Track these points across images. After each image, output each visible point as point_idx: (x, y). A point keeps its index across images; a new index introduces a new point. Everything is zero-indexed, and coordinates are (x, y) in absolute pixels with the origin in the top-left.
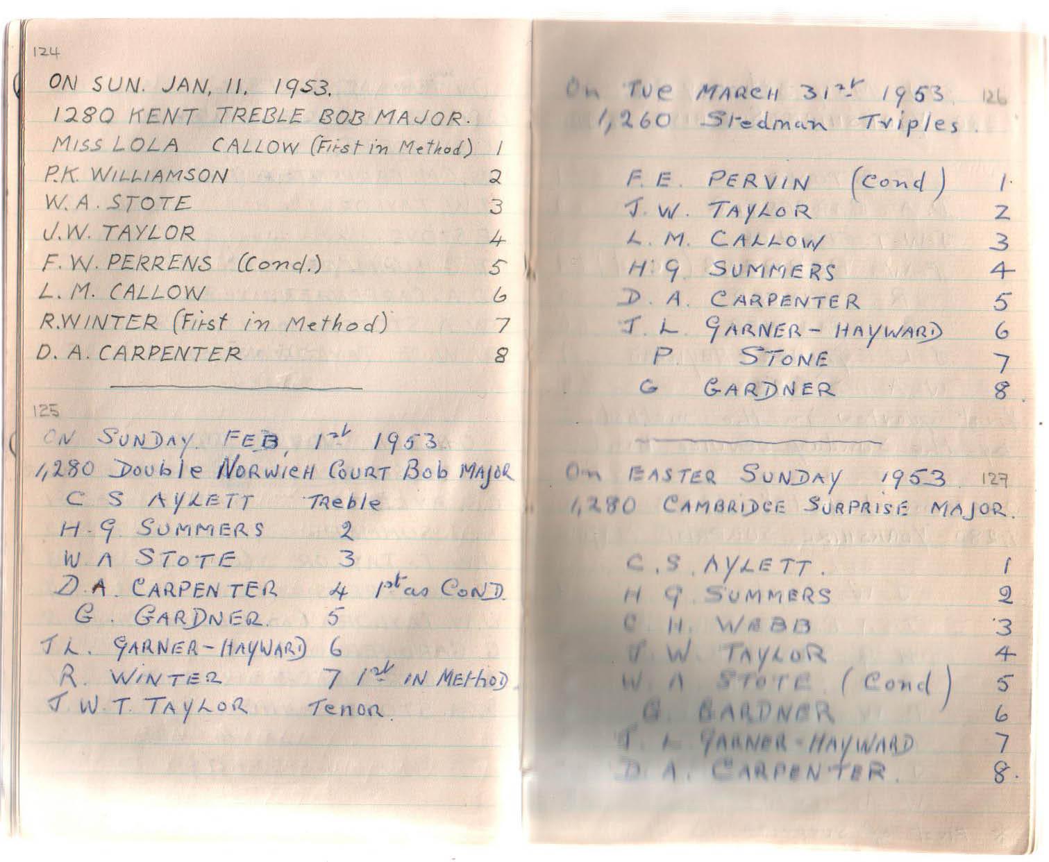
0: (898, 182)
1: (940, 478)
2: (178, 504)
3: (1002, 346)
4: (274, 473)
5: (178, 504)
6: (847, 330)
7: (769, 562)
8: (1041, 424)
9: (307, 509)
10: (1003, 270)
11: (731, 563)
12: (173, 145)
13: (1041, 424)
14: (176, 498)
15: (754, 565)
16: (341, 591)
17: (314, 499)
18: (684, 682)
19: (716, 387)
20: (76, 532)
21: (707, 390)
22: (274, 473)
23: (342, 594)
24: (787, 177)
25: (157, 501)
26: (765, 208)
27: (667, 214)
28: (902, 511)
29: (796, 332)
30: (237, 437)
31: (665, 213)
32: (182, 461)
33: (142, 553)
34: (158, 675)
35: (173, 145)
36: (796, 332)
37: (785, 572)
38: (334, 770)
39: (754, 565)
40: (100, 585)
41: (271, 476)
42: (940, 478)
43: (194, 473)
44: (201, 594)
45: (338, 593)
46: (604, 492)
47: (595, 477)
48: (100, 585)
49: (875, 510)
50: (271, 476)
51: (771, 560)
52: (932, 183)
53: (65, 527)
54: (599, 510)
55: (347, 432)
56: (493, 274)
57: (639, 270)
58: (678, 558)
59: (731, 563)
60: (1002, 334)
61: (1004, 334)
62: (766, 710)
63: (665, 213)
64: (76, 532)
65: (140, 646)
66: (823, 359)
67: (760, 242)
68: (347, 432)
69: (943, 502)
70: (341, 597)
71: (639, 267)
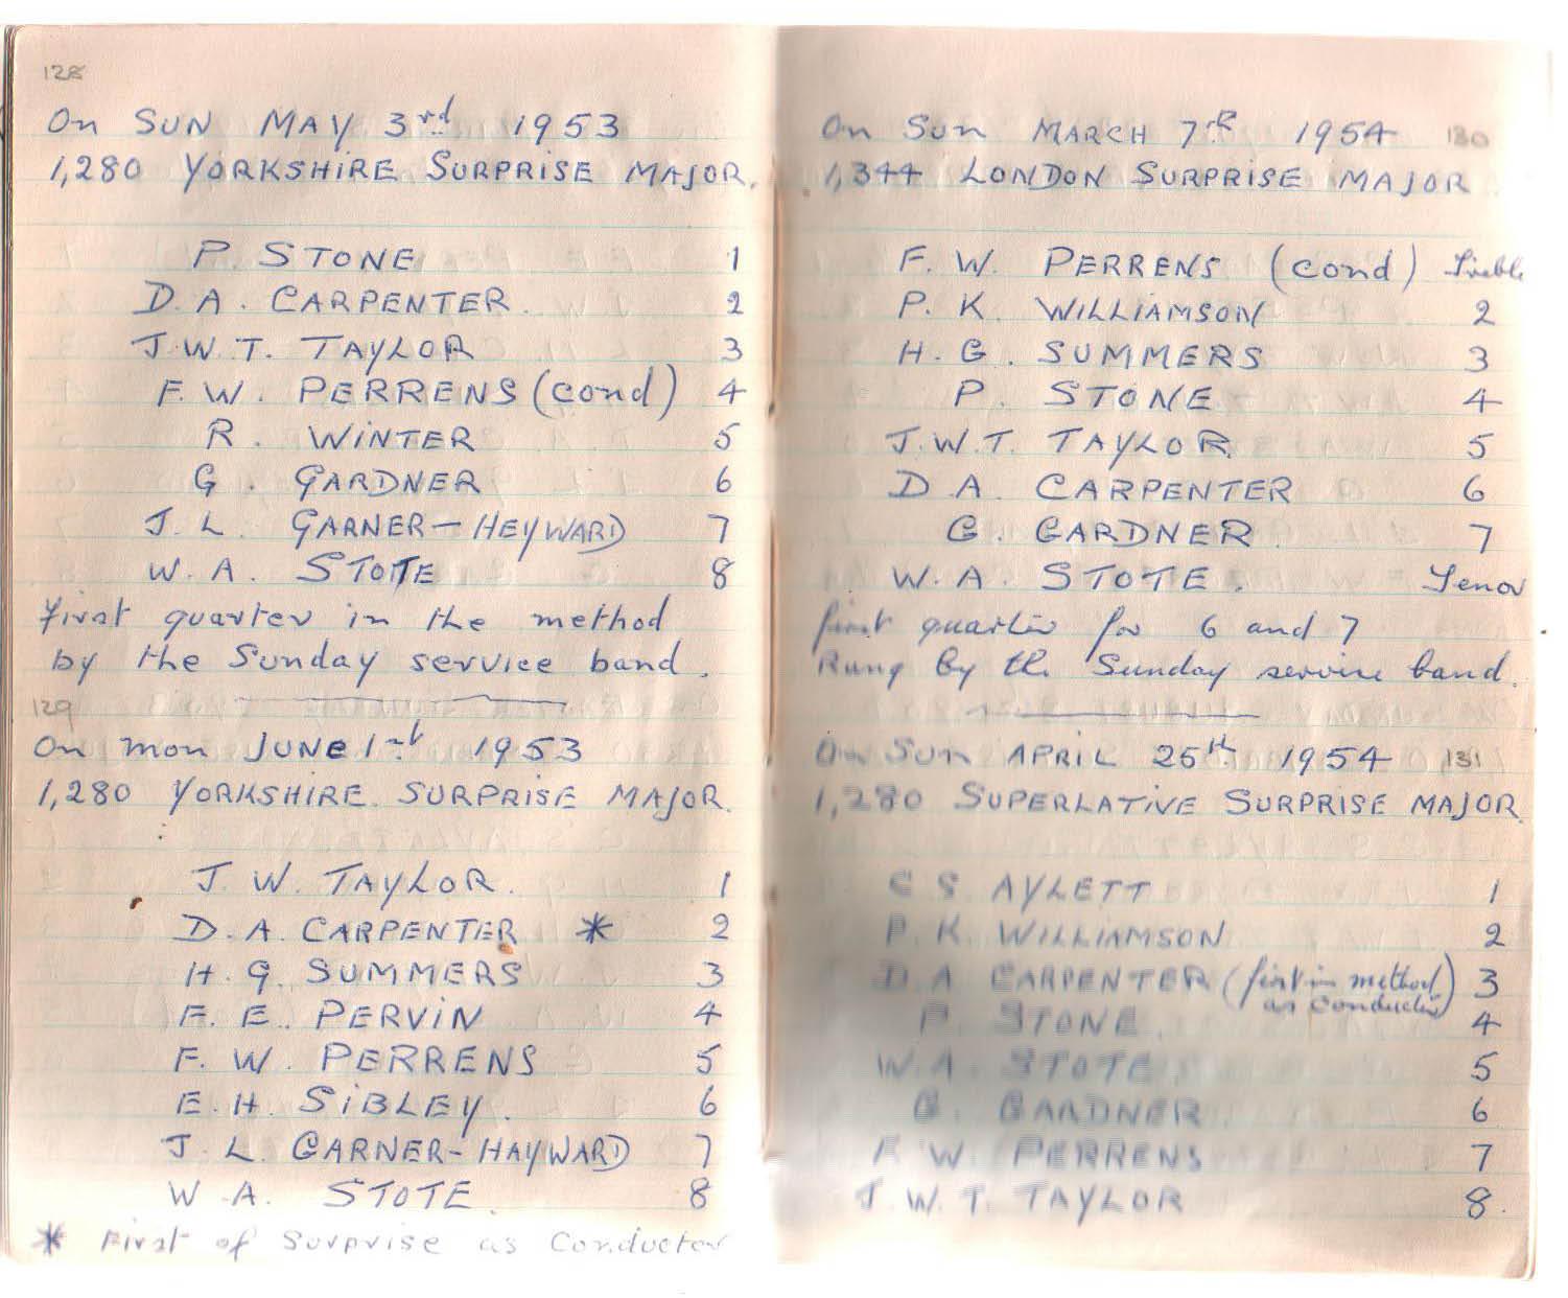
0: (638, 662)
3: (1478, 513)
8: (1544, 632)
10: (1481, 401)
11: (1033, 885)
13: (1544, 632)
15: (1068, 887)
18: (877, 1063)
27: (1058, 314)
28: (565, 801)
31: (1055, 313)
32: (167, 646)
33: (1056, 389)
38: (355, 548)
39: (1068, 887)
43: (189, 666)
44: (255, 1016)
46: (868, 780)
51: (1091, 880)
52: (1398, 270)
54: (867, 807)
55: (1178, 271)
58: (954, 878)
59: (1033, 885)
60: (1472, 495)
61: (1478, 496)
63: (1055, 313)
68: (1178, 271)
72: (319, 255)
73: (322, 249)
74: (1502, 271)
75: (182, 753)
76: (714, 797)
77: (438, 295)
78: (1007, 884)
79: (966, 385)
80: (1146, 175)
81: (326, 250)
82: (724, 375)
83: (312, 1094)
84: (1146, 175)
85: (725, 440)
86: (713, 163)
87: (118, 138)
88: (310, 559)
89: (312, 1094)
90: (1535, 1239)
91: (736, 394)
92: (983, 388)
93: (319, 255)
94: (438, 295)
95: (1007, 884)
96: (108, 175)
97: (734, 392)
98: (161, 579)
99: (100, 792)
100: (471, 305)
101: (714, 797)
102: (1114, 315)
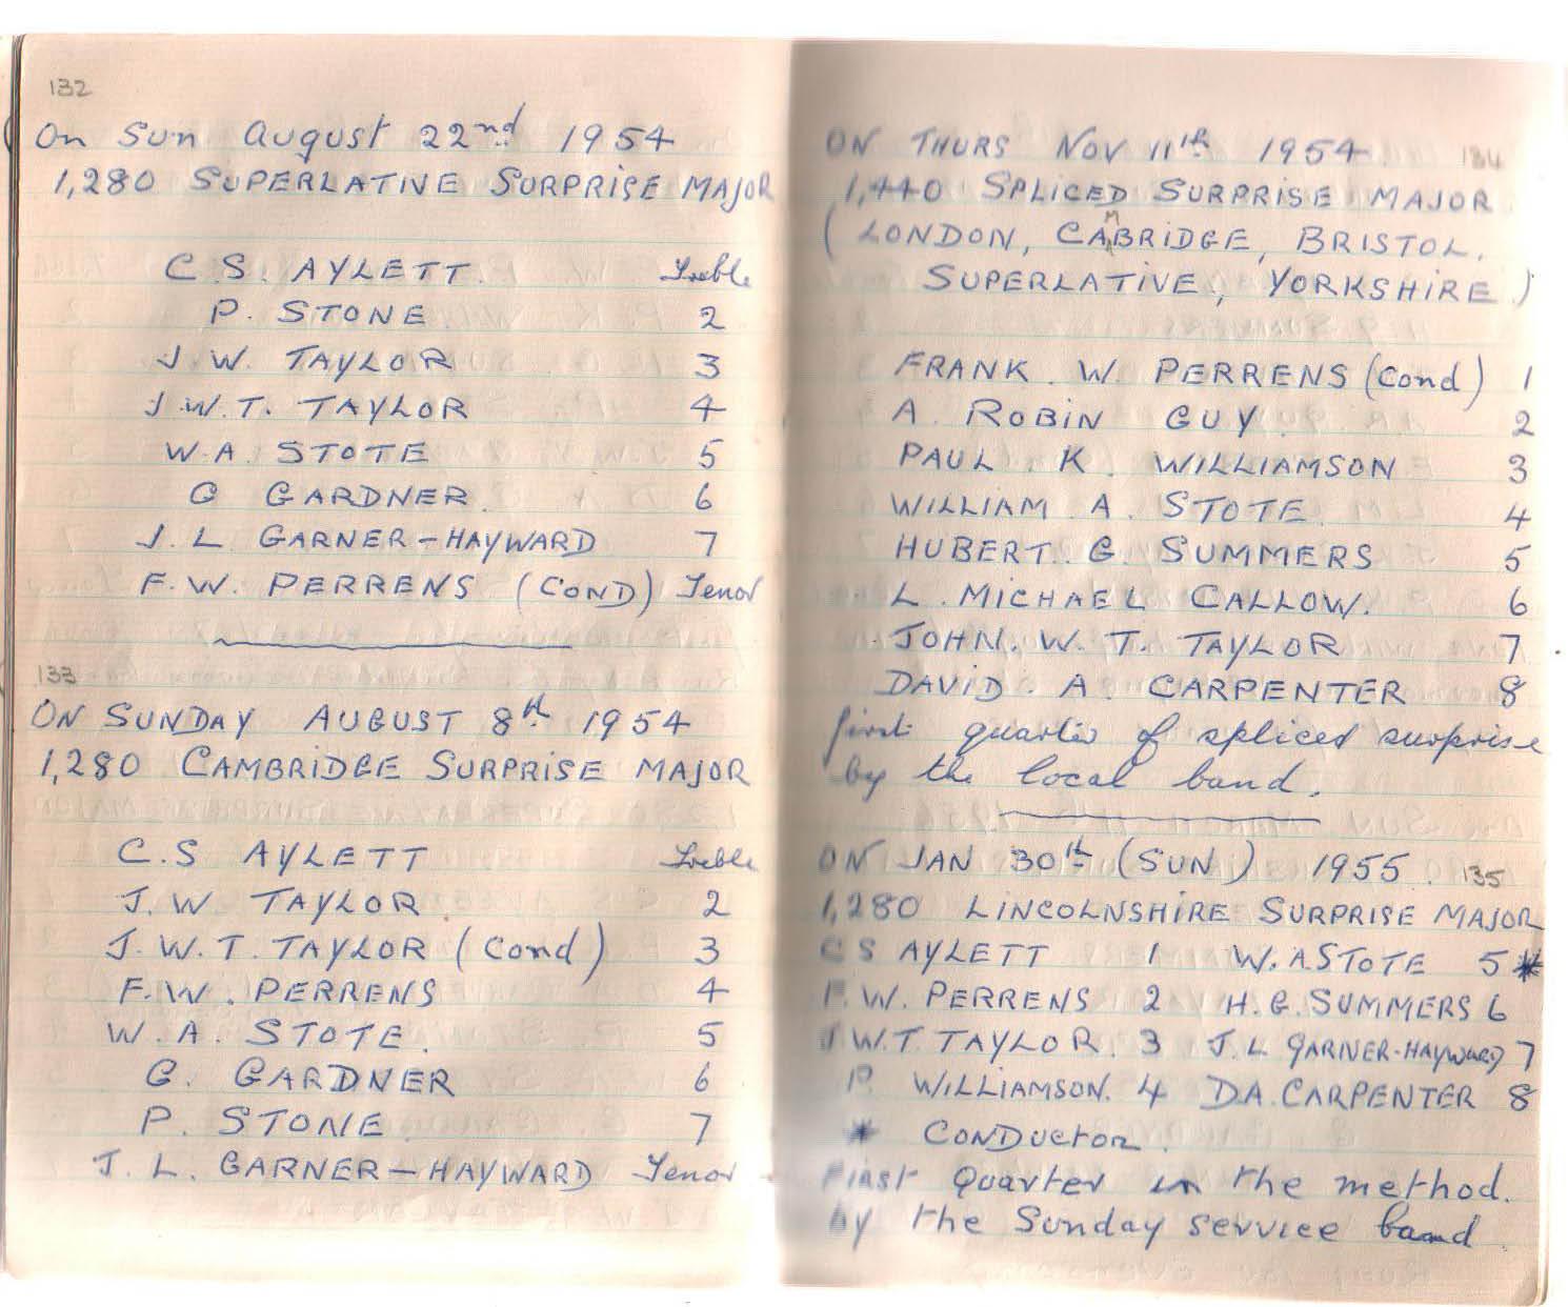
7: (1035, 997)
12: (1077, 686)
16: (1153, 1089)
23: (1155, 1095)
26: (1020, 1038)
29: (596, 188)
35: (1077, 686)
36: (596, 188)
37: (902, 1049)
45: (1149, 1092)
49: (311, 772)
52: (1468, 379)
53: (1233, 1003)
57: (909, 551)
62: (1187, 236)
65: (309, 537)
67: (980, 912)
69: (253, 761)
70: (1153, 1101)
71: (907, 547)
74: (857, 775)
79: (1308, 231)
81: (389, 850)
86: (1276, 1017)
88: (933, 265)
91: (714, 994)
92: (1000, 408)
95: (913, 948)
96: (102, 773)
98: (1055, 648)
99: (501, 721)
100: (983, 956)
102: (972, 912)
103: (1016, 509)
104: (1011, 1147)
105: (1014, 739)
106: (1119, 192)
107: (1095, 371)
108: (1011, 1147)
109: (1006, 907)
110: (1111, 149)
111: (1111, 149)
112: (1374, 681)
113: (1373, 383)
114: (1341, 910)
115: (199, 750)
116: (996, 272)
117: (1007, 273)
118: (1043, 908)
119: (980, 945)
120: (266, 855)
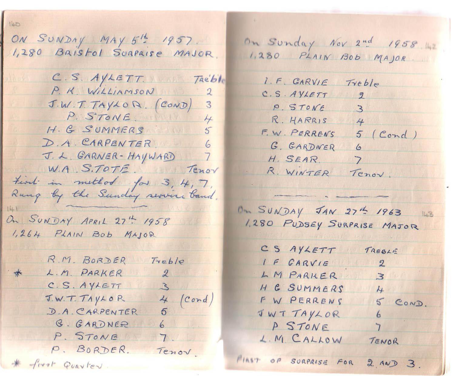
1: (412, 363)
2: (311, 315)
4: (153, 157)
5: (311, 315)
6: (133, 156)
9: (322, 97)
14: (55, 191)
17: (372, 339)
19: (293, 146)
20: (274, 160)
21: (314, 147)
22: (153, 157)
24: (215, 190)
25: (67, 144)
30: (118, 259)
34: (115, 311)
40: (66, 310)
41: (151, 158)
42: (412, 363)
47: (256, 45)
48: (66, 310)
50: (151, 158)
56: (86, 263)
64: (274, 160)
66: (326, 147)
72: (121, 312)
73: (122, 310)
75: (120, 196)
76: (335, 289)
77: (321, 248)
78: (97, 77)
80: (118, 53)
82: (207, 112)
83: (64, 284)
84: (118, 53)
85: (208, 119)
87: (32, 43)
89: (64, 284)
90: (445, 366)
91: (210, 120)
93: (121, 312)
94: (321, 248)
97: (210, 119)
101: (335, 289)
103: (123, 93)
104: (271, 211)
105: (182, 198)
106: (185, 104)
107: (175, 104)
108: (271, 211)
109: (379, 273)
110: (343, 44)
111: (343, 44)
112: (127, 127)
113: (189, 105)
114: (304, 54)
115: (85, 140)
116: (396, 338)
117: (123, 127)
118: (81, 339)
119: (298, 157)
120: (69, 144)
